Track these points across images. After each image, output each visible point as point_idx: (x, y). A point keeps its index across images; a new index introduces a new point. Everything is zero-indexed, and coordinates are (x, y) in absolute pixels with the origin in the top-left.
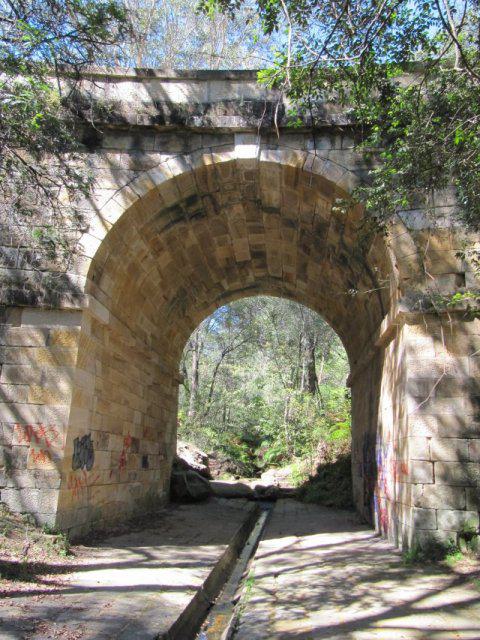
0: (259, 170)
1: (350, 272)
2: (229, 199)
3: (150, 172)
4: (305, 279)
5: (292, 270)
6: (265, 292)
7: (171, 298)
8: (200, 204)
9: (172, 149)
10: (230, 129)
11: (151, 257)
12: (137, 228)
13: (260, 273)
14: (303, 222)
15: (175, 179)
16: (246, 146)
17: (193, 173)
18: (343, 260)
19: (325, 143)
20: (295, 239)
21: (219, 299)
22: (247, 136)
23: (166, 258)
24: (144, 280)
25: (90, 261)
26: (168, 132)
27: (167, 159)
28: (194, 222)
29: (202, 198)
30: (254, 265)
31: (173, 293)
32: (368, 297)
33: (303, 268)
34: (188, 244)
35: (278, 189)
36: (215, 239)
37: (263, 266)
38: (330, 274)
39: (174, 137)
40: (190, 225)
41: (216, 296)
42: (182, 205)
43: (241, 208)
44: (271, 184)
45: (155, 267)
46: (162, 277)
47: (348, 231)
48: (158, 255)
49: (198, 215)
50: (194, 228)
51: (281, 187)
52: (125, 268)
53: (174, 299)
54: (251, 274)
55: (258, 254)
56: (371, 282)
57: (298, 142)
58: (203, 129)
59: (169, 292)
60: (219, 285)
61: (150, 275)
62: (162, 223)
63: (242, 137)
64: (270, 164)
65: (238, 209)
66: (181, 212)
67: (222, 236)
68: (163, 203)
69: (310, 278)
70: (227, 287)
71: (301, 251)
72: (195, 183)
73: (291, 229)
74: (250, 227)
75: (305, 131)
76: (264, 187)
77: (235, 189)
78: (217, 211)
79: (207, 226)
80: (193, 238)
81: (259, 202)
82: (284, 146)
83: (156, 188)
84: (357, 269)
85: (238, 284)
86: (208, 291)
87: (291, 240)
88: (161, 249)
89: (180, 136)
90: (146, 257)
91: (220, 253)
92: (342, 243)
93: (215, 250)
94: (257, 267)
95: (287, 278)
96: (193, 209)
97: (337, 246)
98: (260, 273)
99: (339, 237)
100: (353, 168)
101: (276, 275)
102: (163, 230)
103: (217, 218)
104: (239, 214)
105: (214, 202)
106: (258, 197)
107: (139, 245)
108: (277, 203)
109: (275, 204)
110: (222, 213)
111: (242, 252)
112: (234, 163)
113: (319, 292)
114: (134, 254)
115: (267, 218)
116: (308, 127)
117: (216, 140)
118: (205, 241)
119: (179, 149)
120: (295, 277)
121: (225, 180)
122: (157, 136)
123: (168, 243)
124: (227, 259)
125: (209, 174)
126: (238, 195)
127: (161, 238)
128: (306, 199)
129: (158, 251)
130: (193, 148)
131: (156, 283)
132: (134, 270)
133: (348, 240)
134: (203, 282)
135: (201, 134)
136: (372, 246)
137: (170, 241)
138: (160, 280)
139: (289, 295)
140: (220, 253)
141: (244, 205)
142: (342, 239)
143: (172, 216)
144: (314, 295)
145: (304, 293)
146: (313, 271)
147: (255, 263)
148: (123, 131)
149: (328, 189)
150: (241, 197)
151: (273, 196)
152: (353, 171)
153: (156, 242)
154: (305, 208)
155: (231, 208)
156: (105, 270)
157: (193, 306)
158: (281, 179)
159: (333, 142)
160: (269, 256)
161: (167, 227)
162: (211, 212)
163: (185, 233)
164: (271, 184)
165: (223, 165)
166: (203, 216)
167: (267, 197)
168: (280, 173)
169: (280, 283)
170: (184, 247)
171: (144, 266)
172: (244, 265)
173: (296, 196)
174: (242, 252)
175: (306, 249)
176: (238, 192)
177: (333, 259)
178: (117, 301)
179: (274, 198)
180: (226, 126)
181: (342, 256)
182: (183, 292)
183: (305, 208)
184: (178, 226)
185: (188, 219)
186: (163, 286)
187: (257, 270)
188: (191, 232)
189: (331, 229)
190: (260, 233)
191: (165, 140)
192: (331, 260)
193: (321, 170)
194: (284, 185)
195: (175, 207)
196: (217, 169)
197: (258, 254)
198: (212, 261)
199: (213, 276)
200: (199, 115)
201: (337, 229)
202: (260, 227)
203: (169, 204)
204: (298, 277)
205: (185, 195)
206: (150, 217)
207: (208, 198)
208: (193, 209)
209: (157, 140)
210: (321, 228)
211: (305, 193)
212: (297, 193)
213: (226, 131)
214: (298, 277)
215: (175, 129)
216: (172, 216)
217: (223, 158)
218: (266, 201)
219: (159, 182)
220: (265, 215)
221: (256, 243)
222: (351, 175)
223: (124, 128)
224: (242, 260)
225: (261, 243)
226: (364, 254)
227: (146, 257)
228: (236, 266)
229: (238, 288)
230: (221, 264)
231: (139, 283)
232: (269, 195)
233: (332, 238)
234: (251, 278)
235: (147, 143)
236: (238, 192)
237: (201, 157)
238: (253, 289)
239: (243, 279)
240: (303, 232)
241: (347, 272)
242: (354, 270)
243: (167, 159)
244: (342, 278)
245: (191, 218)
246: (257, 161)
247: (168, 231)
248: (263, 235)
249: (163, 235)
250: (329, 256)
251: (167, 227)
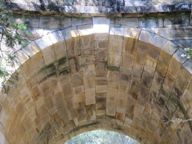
0: (108, 41)
1: (166, 110)
2: (87, 61)
3: (37, 41)
4: (132, 117)
5: (122, 111)
6: (102, 127)
7: (40, 131)
8: (67, 64)
9: (51, 27)
10: (90, 14)
11: (32, 100)
12: (26, 79)
13: (101, 113)
14: (135, 76)
15: (53, 47)
16: (92, 33)
17: (66, 42)
18: (162, 102)
19: (152, 22)
20: (127, 89)
21: (71, 132)
22: (101, 19)
23: (41, 101)
24: (26, 117)
25: (36, 51)
26: (48, 16)
27: (48, 33)
28: (62, 76)
29: (70, 59)
30: (97, 108)
31: (43, 127)
32: (180, 127)
33: (132, 109)
34: (56, 92)
35: (120, 54)
36: (74, 89)
37: (103, 108)
38: (150, 112)
39: (52, 19)
40: (59, 78)
41: (69, 130)
42: (56, 64)
43: (94, 66)
44: (116, 50)
45: (33, 108)
46: (37, 115)
47: (166, 81)
48: (37, 99)
49: (65, 72)
50: (61, 81)
51: (122, 53)
52: (15, 107)
53: (43, 131)
54: (94, 114)
55: (101, 100)
56: (183, 116)
57: (134, 23)
58: (72, 14)
59: (40, 126)
60: (72, 121)
61: (30, 113)
62: (42, 76)
63: (98, 19)
64: (116, 37)
65: (92, 68)
66: (55, 69)
67: (79, 87)
68: (44, 62)
69: (135, 116)
70: (77, 124)
71: (131, 97)
72: (65, 50)
73: (126, 82)
74: (98, 81)
75: (139, 16)
76: (111, 53)
77: (91, 54)
78: (77, 70)
79: (69, 78)
80: (60, 87)
81: (106, 63)
82: (125, 25)
83: (41, 52)
84: (172, 107)
85: (84, 121)
86: (65, 126)
87: (125, 89)
88: (39, 95)
89: (56, 19)
90: (29, 100)
91: (76, 99)
92: (162, 91)
93: (72, 97)
94: (99, 109)
95: (118, 116)
96: (62, 67)
97: (158, 92)
98: (101, 113)
99: (160, 86)
100: (172, 39)
101: (112, 115)
102: (41, 82)
103: (78, 74)
104: (91, 71)
105: (76, 64)
106: (106, 59)
107: (26, 91)
108: (119, 63)
109: (117, 64)
110: (80, 70)
111: (91, 99)
112: (92, 36)
113: (141, 126)
114: (22, 97)
115: (110, 74)
116: (141, 13)
117: (80, 21)
118: (67, 90)
119: (56, 26)
120: (124, 116)
121: (87, 47)
122: (41, 18)
123: (44, 91)
124: (80, 103)
125: (75, 43)
126: (92, 58)
127: (40, 87)
128: (138, 61)
129: (36, 96)
130: (65, 26)
131: (33, 119)
132: (21, 108)
133: (166, 88)
134: (62, 119)
135: (71, 17)
136: (186, 90)
137: (45, 89)
138: (35, 117)
139: (119, 129)
140: (76, 99)
141: (95, 65)
142: (162, 87)
143: (49, 71)
144: (137, 128)
145: (129, 127)
146: (139, 110)
147: (98, 106)
148: (18, 14)
149: (154, 52)
150: (94, 59)
151: (116, 59)
152: (171, 41)
153: (36, 89)
154: (137, 67)
155: (87, 67)
156: (3, 107)
157: (53, 137)
158: (123, 46)
159: (157, 23)
160: (108, 101)
161: (45, 79)
162: (74, 70)
163: (55, 84)
164: (116, 50)
165: (85, 37)
166: (68, 73)
167: (111, 60)
168: (123, 43)
169: (113, 120)
170: (53, 94)
171: (27, 106)
172: (90, 108)
173: (132, 59)
174: (91, 99)
175: (135, 96)
176: (93, 56)
177: (154, 101)
178: (8, 131)
179: (116, 60)
180: (88, 12)
181: (161, 99)
182: (49, 126)
183: (137, 67)
184: (53, 78)
185: (58, 74)
186: (37, 121)
187: (99, 111)
188: (59, 84)
189: (154, 80)
190: (104, 84)
191: (47, 21)
192: (152, 102)
193: (151, 41)
194: (124, 51)
195: (51, 66)
196: (80, 40)
197: (101, 100)
198: (70, 104)
199: (69, 115)
200: (68, 5)
201: (159, 80)
202: (104, 80)
203: (47, 63)
204: (127, 115)
205: (59, 58)
206: (35, 71)
207: (73, 60)
208: (62, 67)
209: (41, 21)
210: (146, 81)
211: (138, 56)
212: (132, 56)
213: (87, 16)
214: (127, 115)
215: (54, 14)
216: (49, 71)
217: (84, 32)
218: (110, 62)
219: (42, 48)
220: (109, 72)
221: (101, 92)
222: (171, 43)
223: (19, 13)
224: (90, 104)
225: (103, 92)
226: (178, 97)
227: (29, 100)
228: (85, 108)
229: (84, 124)
230: (75, 107)
231: (23, 118)
232: (113, 58)
233: (155, 87)
234: (93, 118)
235: (34, 22)
236: (93, 56)
237: (69, 33)
238: (95, 125)
239: (89, 117)
240: (134, 83)
241: (164, 110)
242: (170, 108)
243: (48, 33)
244: (160, 115)
245: (61, 73)
246: (109, 36)
247: (44, 82)
248: (106, 86)
249: (41, 85)
250: (151, 100)
251: (45, 79)
